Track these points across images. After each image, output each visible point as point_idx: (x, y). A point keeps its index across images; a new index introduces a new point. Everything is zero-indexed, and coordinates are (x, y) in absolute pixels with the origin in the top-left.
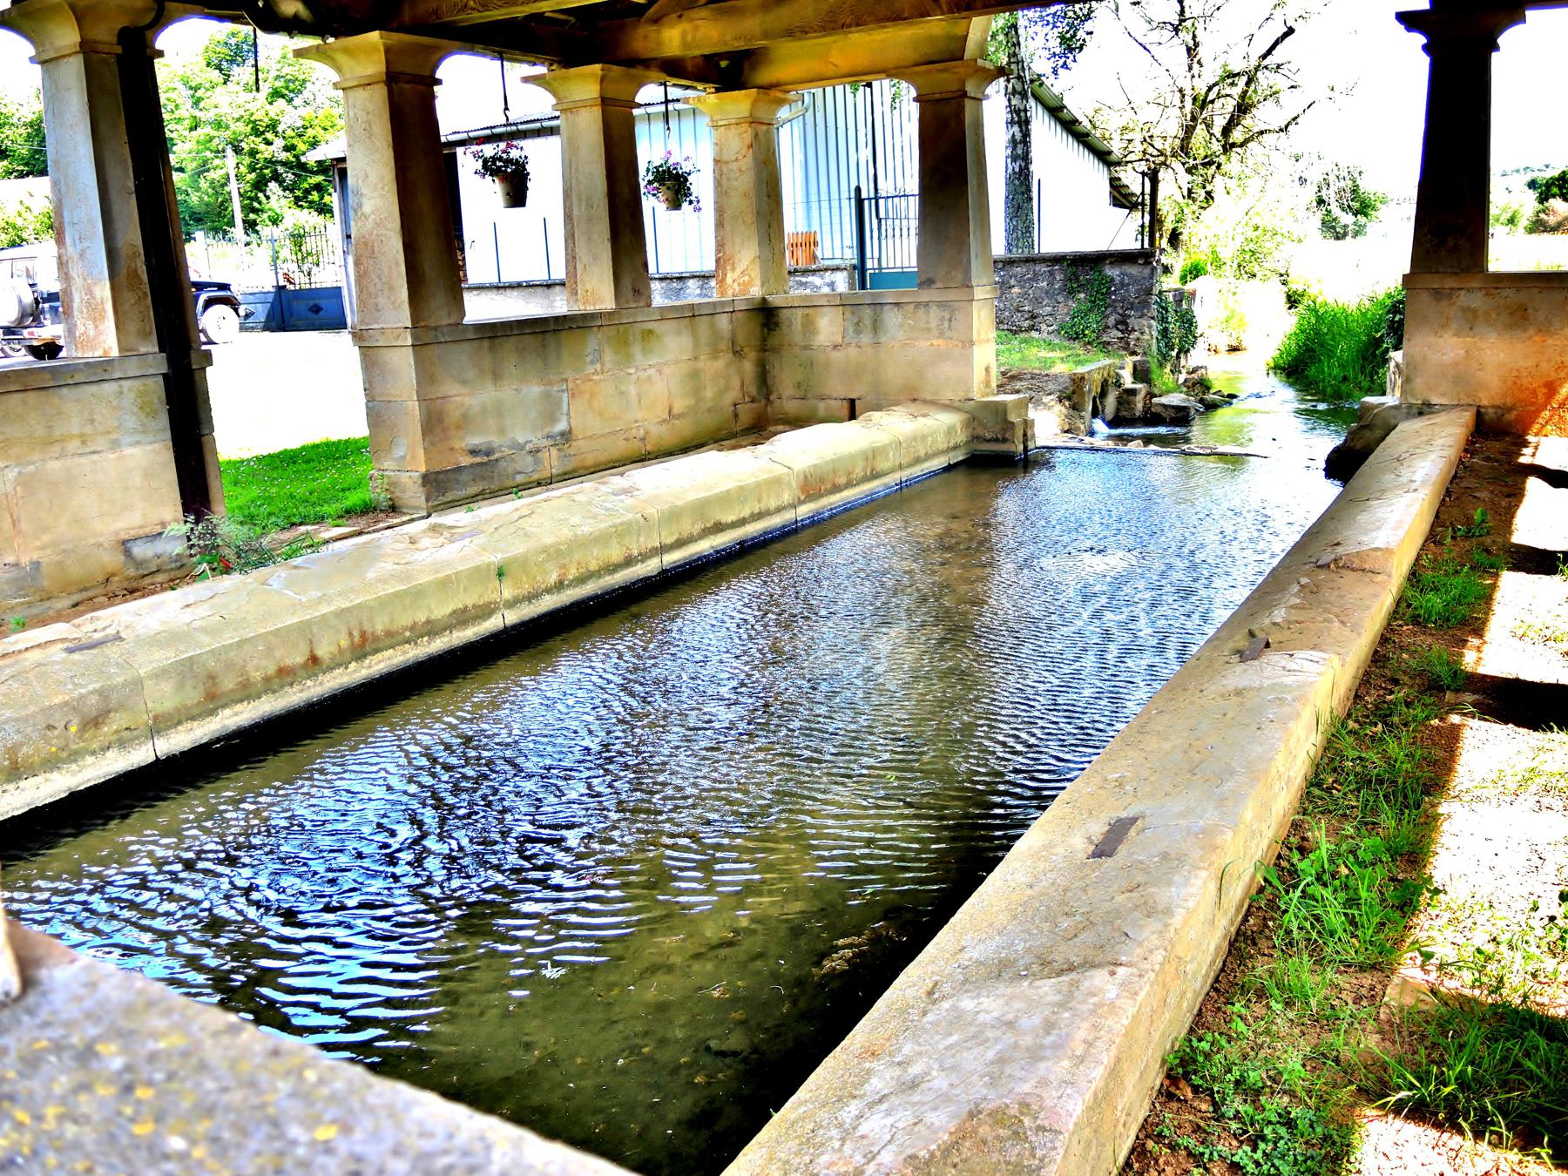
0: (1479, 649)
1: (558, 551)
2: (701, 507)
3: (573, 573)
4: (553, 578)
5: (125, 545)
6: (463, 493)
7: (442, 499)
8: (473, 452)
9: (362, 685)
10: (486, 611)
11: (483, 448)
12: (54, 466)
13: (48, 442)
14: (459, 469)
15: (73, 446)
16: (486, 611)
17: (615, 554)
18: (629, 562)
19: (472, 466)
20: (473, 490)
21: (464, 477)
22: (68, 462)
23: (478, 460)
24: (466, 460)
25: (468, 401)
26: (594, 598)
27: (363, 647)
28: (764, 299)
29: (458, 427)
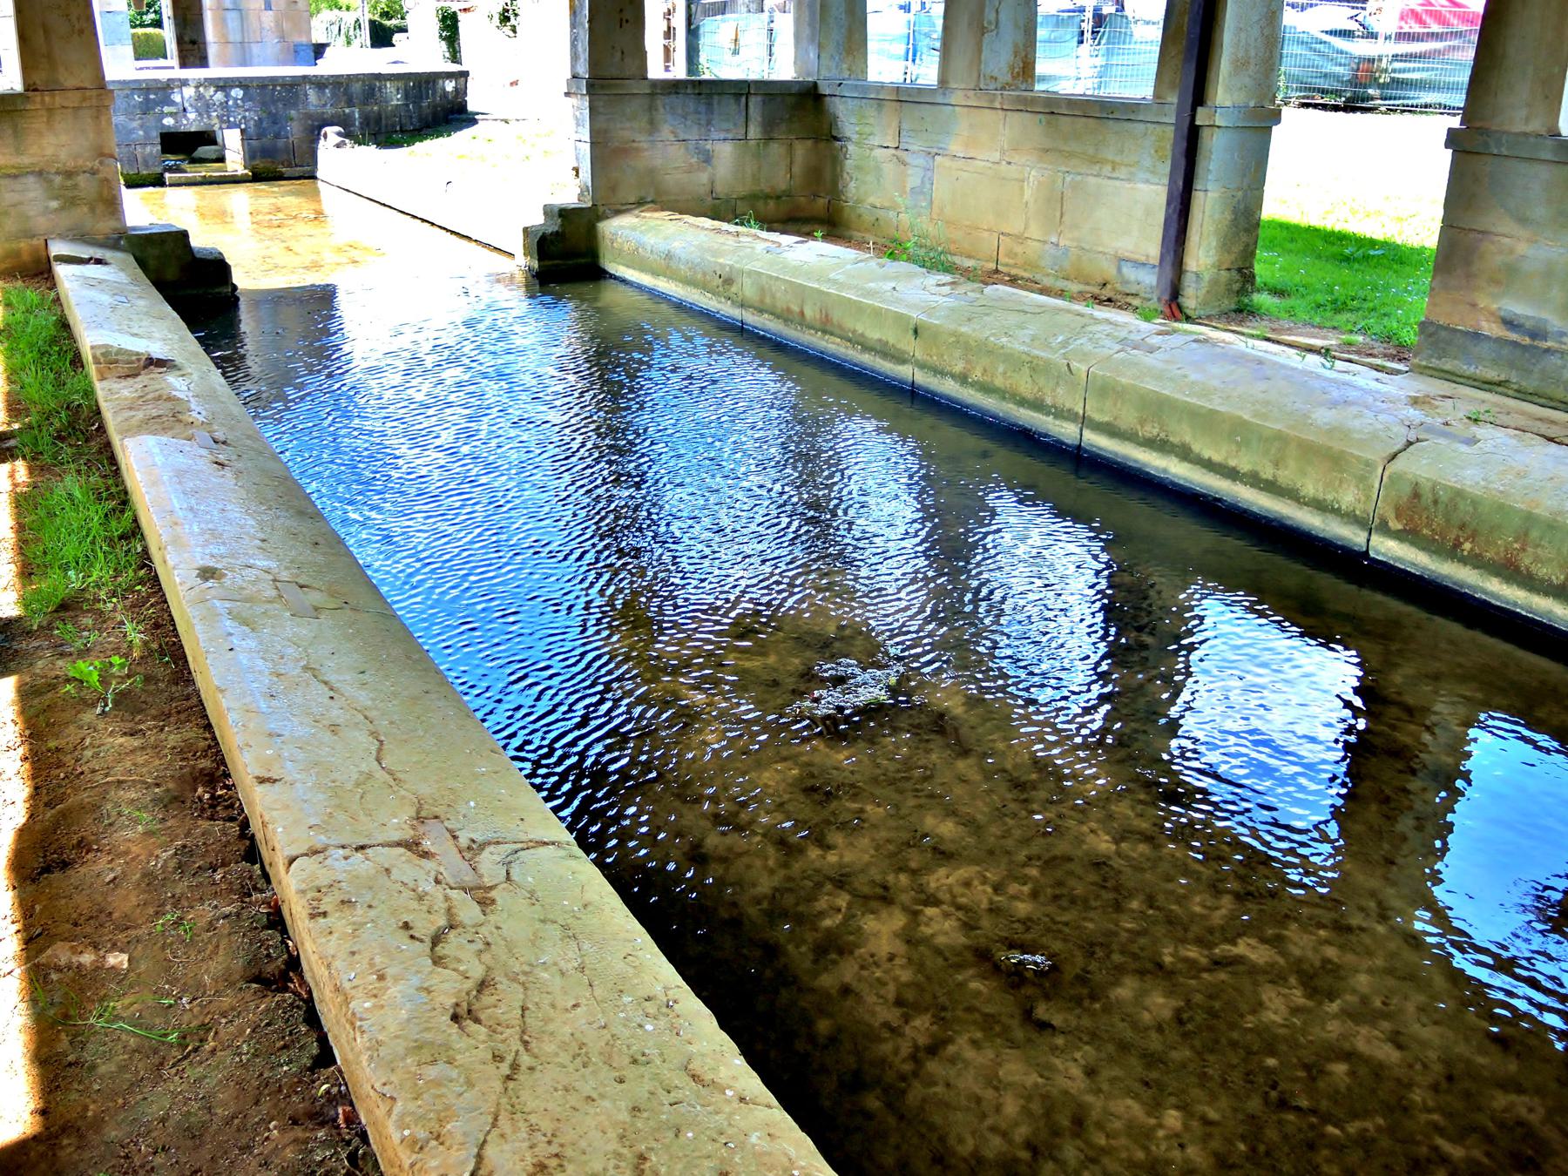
0: (16, 485)
1: (967, 343)
2: (1156, 406)
3: (977, 375)
4: (958, 368)
5: (1121, 260)
6: (1470, 370)
7: (1435, 363)
8: (1509, 323)
9: (1323, 540)
10: (901, 359)
11: (1528, 324)
12: (1092, 180)
13: (1094, 160)
14: (1476, 336)
15: (1107, 169)
16: (901, 359)
17: (1025, 387)
18: (1038, 405)
19: (1498, 340)
20: (1492, 374)
21: (1484, 349)
22: (1099, 180)
23: (1514, 336)
24: (1491, 329)
25: (1522, 248)
26: (984, 412)
27: (826, 328)
28: (815, 84)
29: (1495, 282)
